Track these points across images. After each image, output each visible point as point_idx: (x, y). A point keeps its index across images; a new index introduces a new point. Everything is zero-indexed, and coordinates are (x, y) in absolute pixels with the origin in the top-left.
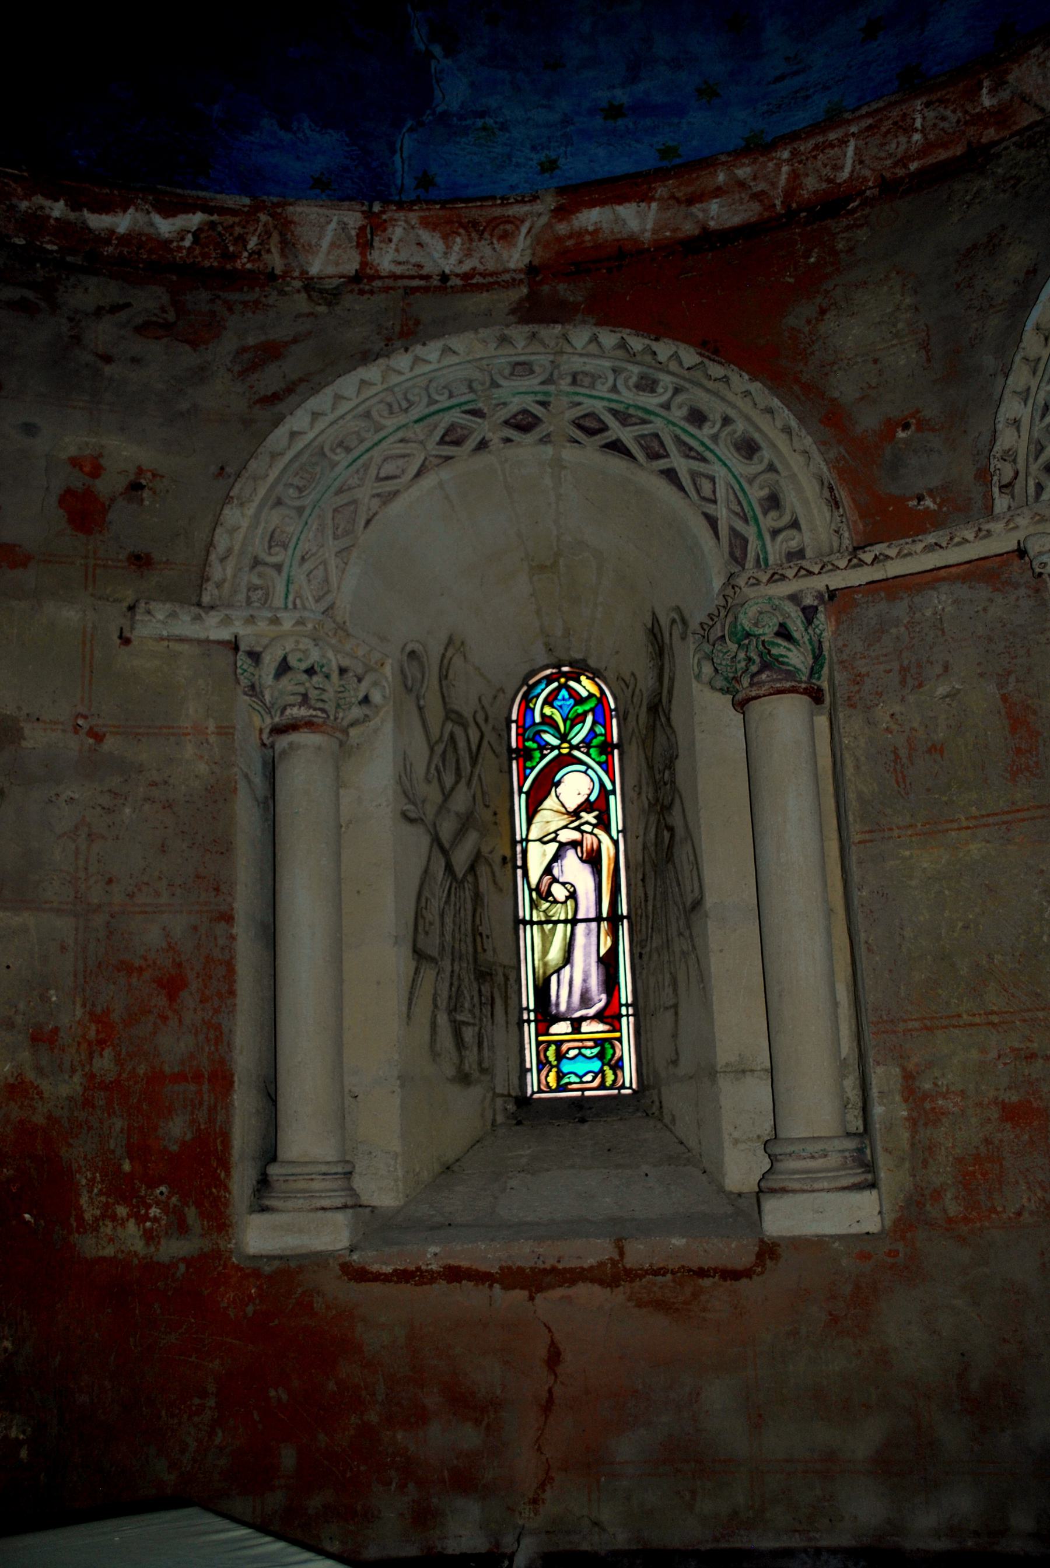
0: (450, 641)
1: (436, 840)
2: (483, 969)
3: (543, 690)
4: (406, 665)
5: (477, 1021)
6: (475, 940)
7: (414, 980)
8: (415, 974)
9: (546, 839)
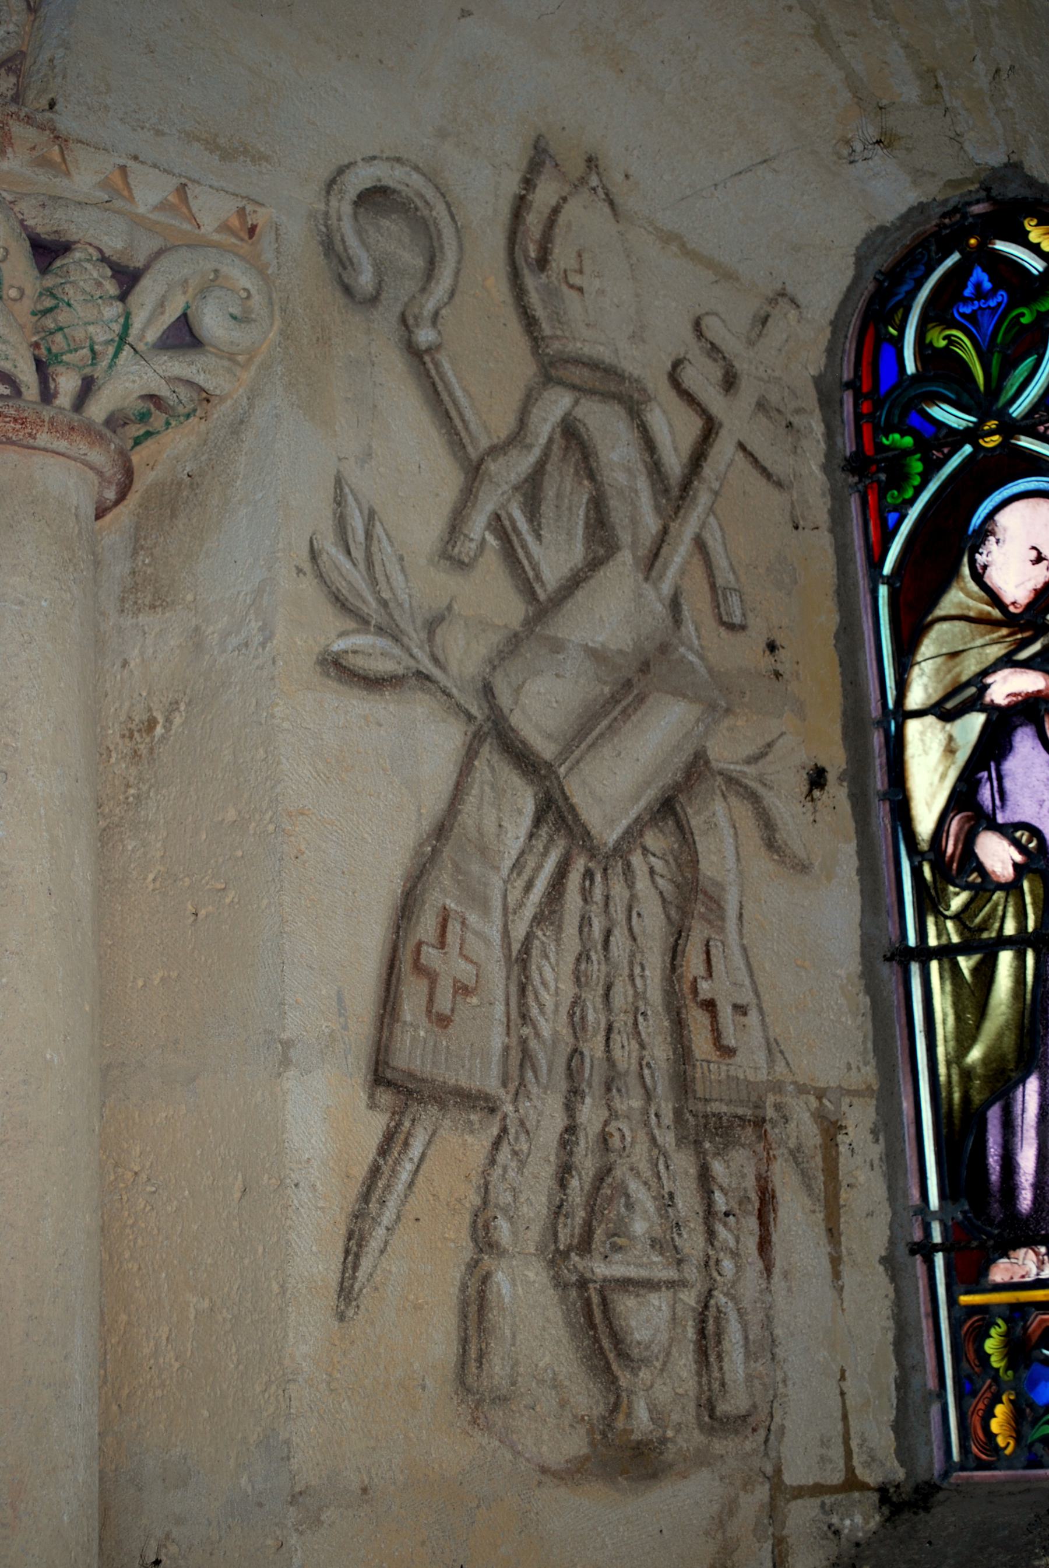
0: (539, 159)
1: (496, 734)
2: (715, 1107)
4: (347, 227)
5: (692, 1273)
6: (679, 1024)
7: (375, 1171)
8: (383, 1151)
9: (949, 705)
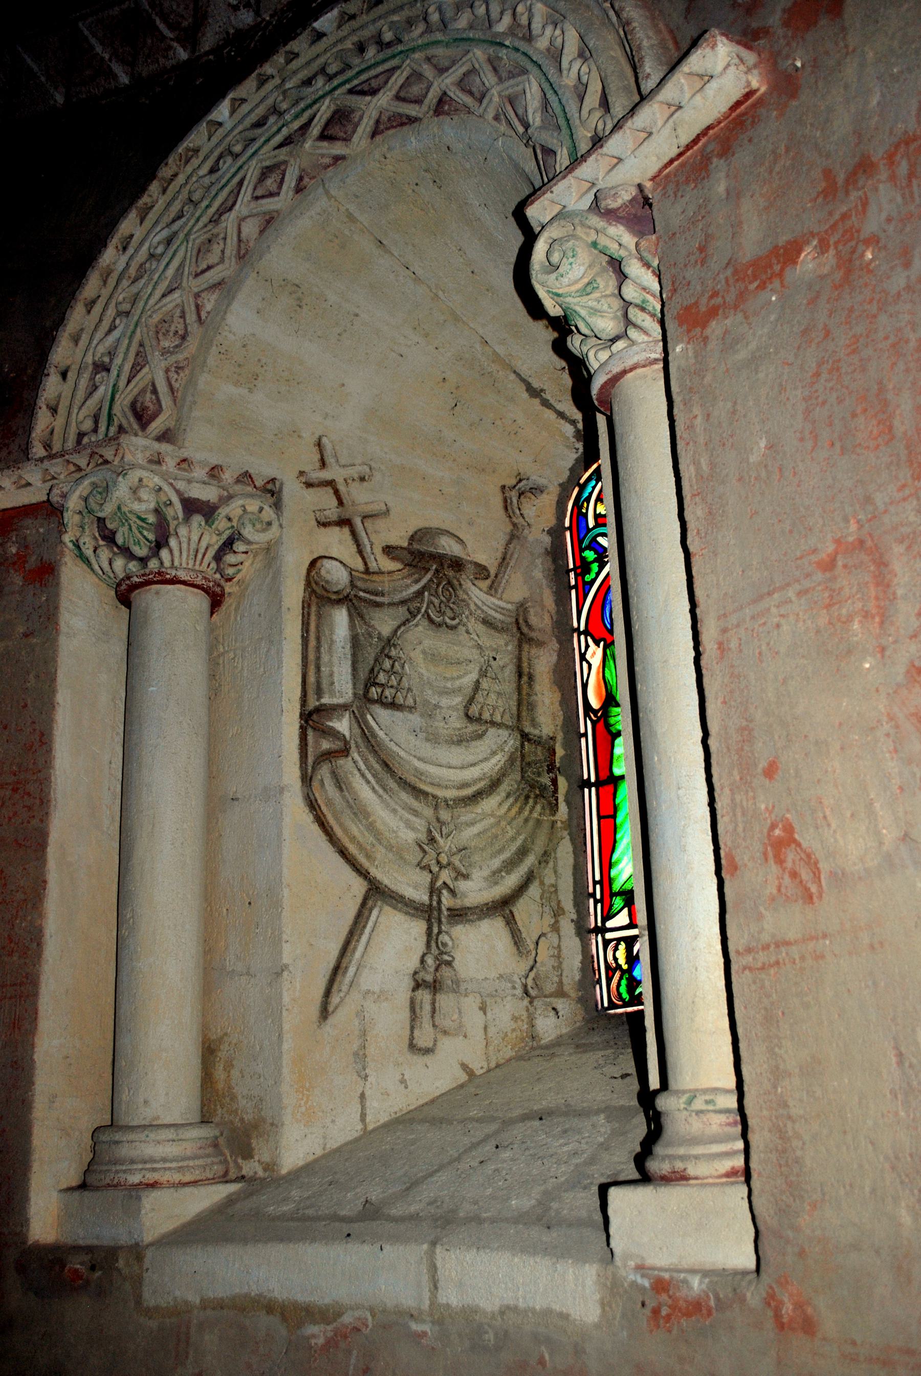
3: (594, 488)
